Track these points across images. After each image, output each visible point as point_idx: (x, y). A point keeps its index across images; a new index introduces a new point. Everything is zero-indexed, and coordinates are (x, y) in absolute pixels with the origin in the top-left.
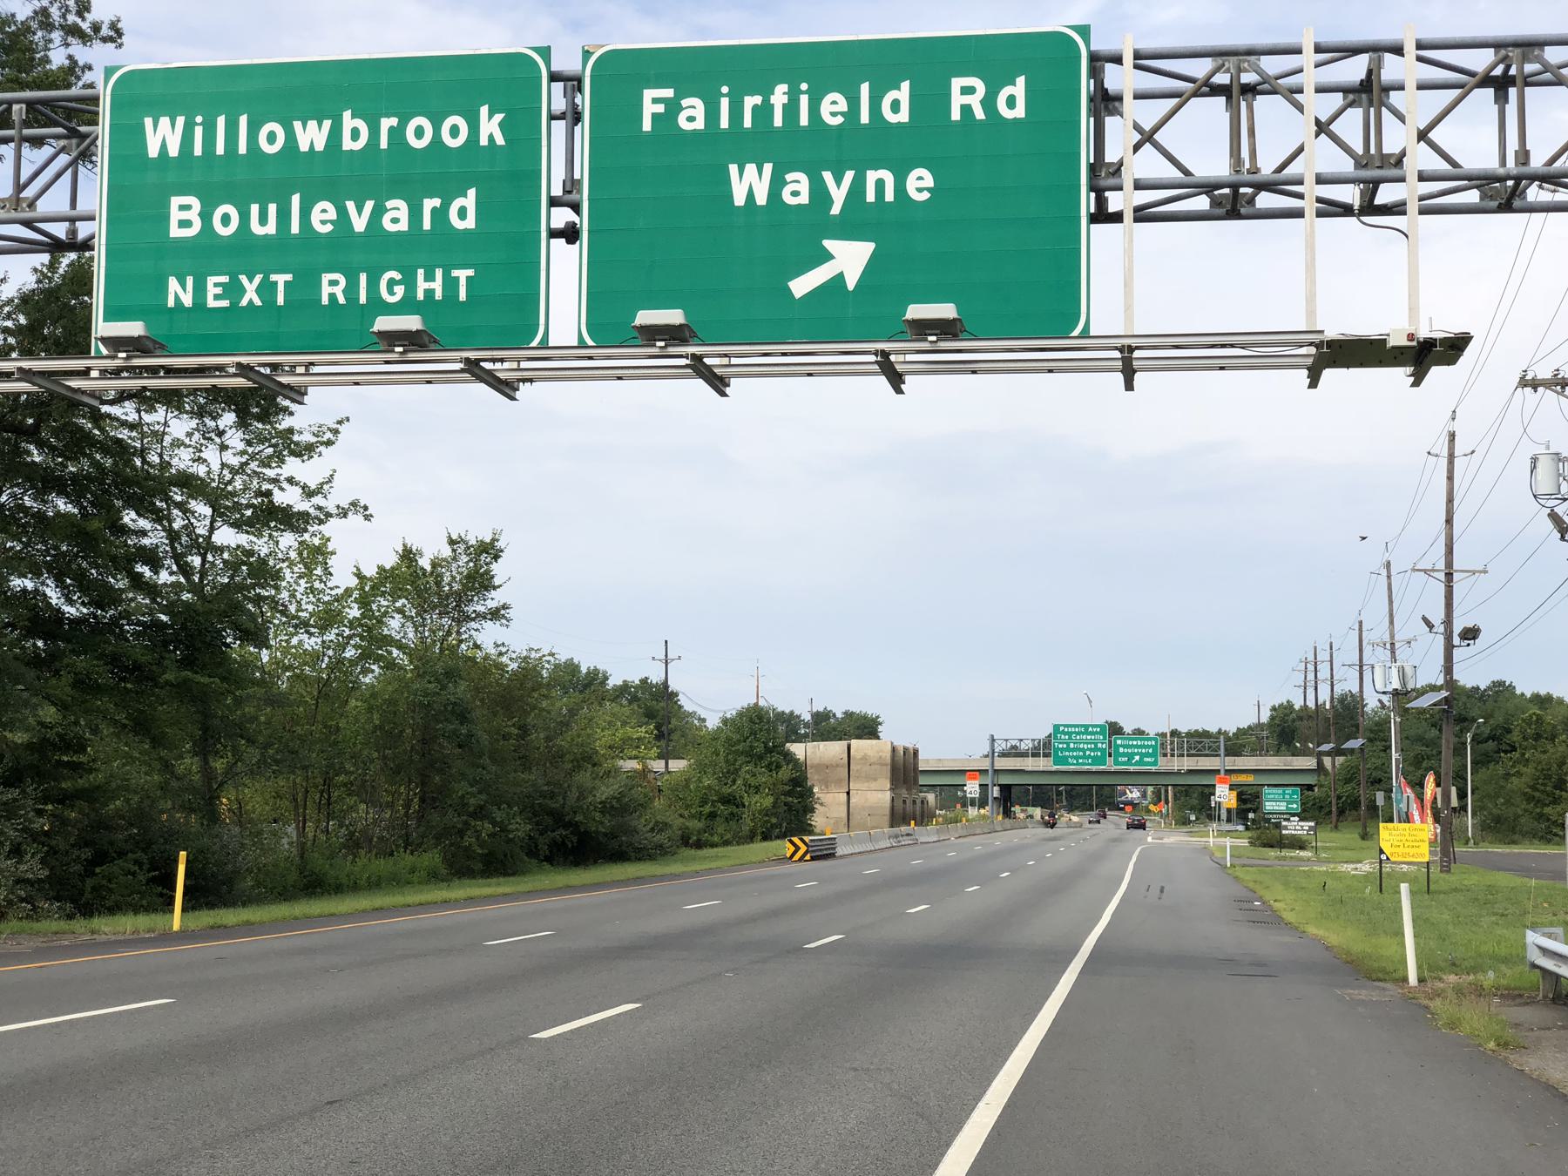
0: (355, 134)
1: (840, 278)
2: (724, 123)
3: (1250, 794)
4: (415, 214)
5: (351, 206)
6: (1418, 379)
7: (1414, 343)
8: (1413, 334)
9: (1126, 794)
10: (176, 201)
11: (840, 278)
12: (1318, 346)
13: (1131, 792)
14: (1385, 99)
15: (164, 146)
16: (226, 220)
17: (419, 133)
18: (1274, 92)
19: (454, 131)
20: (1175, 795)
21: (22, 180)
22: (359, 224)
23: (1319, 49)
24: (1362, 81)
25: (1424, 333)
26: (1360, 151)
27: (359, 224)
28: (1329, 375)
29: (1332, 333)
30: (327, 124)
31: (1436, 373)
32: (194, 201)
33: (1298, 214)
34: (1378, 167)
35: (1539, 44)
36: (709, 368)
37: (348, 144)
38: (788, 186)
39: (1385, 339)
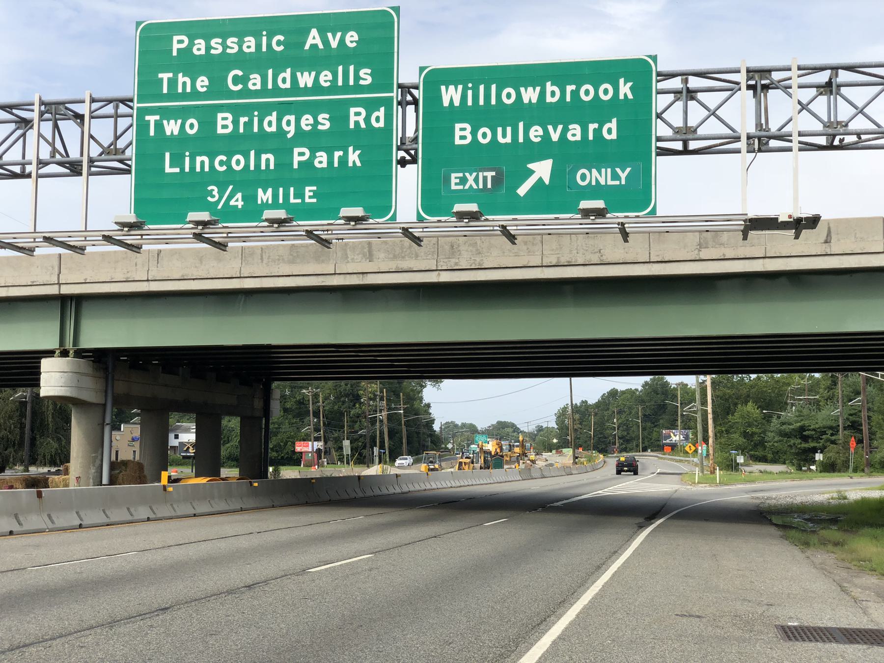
0: (553, 94)
1: (540, 179)
2: (481, 102)
3: (814, 430)
4: (585, 131)
5: (550, 128)
6: (797, 237)
7: (792, 220)
8: (791, 215)
9: (670, 437)
10: (458, 126)
11: (540, 179)
12: (745, 221)
13: (675, 436)
14: (839, 92)
15: (451, 100)
16: (484, 135)
17: (587, 93)
18: (777, 88)
19: (606, 92)
20: (716, 435)
21: (118, 134)
22: (555, 137)
23: (800, 68)
24: (826, 82)
25: (796, 215)
26: (826, 119)
27: (555, 137)
28: (752, 233)
29: (751, 215)
30: (538, 89)
31: (805, 233)
32: (468, 126)
33: (790, 150)
34: (684, 133)
35: (769, 71)
36: (411, 233)
37: (549, 99)
38: (570, 132)
39: (778, 218)
